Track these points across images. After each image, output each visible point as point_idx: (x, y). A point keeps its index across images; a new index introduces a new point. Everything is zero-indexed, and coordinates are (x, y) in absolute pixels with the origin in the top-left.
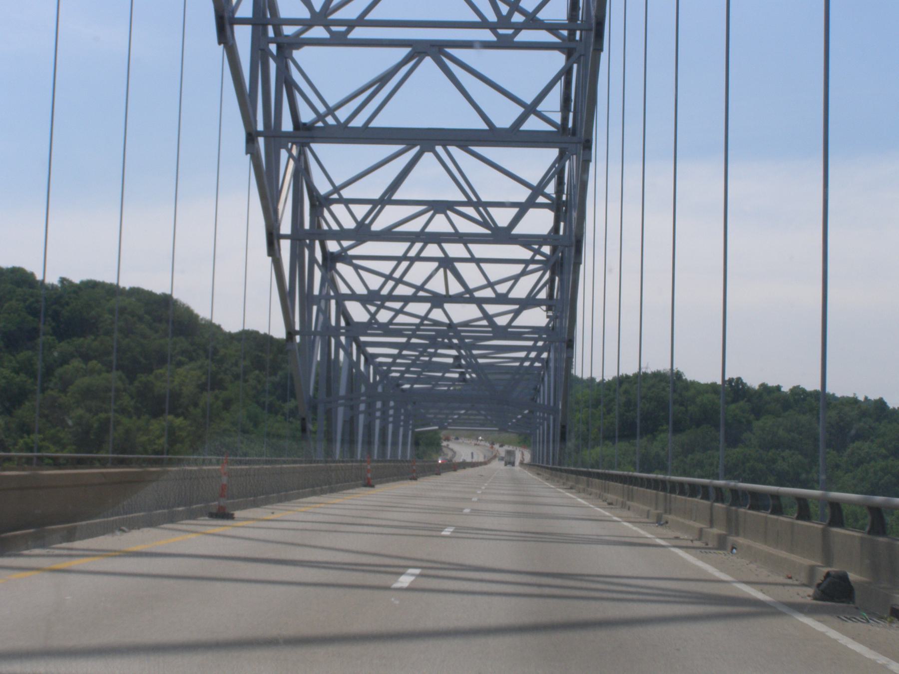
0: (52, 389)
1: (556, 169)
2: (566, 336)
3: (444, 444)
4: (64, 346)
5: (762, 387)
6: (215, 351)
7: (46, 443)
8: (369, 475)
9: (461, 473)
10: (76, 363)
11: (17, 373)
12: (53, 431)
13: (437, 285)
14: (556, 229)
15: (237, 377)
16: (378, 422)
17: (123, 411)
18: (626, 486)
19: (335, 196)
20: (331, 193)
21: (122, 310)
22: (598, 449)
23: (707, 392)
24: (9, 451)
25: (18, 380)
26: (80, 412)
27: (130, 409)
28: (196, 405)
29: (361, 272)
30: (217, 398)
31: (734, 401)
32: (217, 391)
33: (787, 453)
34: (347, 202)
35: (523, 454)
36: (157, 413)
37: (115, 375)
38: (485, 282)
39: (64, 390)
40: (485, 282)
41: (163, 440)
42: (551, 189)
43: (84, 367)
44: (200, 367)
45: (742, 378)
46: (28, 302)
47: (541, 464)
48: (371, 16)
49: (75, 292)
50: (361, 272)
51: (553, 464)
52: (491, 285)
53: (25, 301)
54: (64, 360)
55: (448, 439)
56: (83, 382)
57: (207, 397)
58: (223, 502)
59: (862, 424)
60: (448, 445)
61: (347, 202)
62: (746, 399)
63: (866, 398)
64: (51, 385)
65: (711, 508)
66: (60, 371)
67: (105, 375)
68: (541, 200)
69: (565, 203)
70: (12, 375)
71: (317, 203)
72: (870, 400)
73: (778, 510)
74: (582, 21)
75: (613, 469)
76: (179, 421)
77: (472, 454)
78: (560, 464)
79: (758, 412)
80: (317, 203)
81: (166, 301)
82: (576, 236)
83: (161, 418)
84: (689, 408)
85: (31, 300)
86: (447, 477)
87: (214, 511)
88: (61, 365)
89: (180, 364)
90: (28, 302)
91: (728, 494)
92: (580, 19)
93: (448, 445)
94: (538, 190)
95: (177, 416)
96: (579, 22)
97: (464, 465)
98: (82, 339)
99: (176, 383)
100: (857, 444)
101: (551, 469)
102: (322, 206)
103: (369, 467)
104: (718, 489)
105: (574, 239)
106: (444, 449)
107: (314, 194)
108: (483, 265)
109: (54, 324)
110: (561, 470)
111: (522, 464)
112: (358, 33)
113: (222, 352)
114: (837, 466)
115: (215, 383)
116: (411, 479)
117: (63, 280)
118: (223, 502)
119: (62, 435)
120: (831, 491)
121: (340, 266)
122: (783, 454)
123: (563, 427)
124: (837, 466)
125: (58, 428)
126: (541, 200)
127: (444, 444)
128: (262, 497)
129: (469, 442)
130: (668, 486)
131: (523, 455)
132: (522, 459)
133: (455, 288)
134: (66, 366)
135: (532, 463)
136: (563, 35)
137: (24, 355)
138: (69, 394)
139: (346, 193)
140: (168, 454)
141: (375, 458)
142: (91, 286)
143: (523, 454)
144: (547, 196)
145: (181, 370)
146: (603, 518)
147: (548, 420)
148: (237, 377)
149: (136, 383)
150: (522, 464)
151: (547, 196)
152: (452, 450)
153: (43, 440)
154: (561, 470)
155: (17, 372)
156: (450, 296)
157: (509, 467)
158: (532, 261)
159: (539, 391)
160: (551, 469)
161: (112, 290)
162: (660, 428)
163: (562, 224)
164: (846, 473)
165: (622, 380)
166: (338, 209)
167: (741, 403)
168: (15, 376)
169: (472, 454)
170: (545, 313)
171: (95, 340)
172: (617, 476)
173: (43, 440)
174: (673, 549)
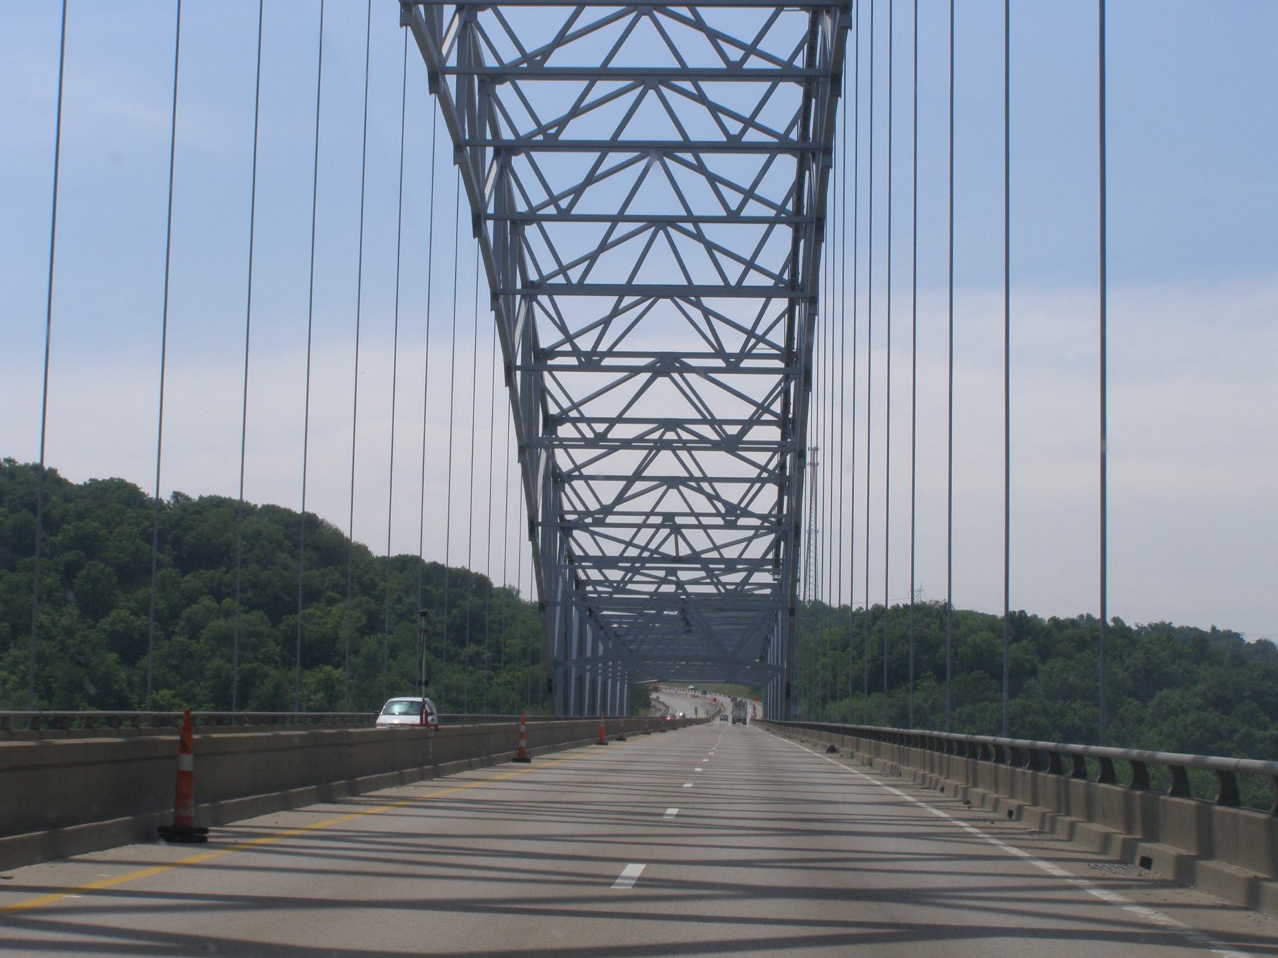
0: (180, 635)
1: (782, 388)
2: (789, 605)
3: (654, 695)
4: (191, 581)
5: (1052, 622)
6: (374, 585)
7: (177, 700)
8: (523, 743)
9: (689, 728)
10: (207, 601)
11: (137, 615)
12: (185, 686)
13: (669, 549)
14: (779, 503)
15: (401, 617)
16: (588, 675)
17: (268, 660)
18: (902, 747)
19: (577, 473)
20: (573, 470)
21: (258, 534)
22: (846, 702)
23: (981, 630)
24: (135, 710)
25: (139, 622)
26: (217, 662)
27: (277, 658)
28: (356, 651)
29: (596, 537)
30: (380, 642)
31: (1017, 639)
32: (379, 635)
33: (1078, 705)
34: (587, 479)
35: (754, 708)
36: (308, 664)
37: (256, 616)
38: (711, 546)
39: (194, 635)
40: (711, 546)
41: (320, 695)
42: (777, 407)
43: (217, 606)
44: (357, 606)
45: (1026, 611)
46: (142, 526)
47: (771, 720)
48: (617, 349)
49: (198, 512)
50: (596, 537)
51: (781, 719)
52: (716, 548)
53: (138, 525)
54: (191, 599)
55: (656, 690)
56: (220, 624)
57: (370, 642)
58: (622, 734)
59: (1175, 667)
60: (658, 698)
61: (587, 479)
62: (1030, 638)
63: (1214, 628)
64: (177, 629)
65: (924, 752)
66: (187, 612)
67: (244, 616)
68: (767, 417)
69: (789, 479)
70: (132, 617)
71: (559, 480)
72: (1218, 631)
73: (1000, 758)
74: (797, 349)
75: (862, 723)
76: (337, 673)
77: (696, 709)
78: (786, 719)
79: (1045, 653)
80: (559, 480)
81: (310, 522)
82: (795, 523)
83: (316, 669)
84: (959, 649)
85: (147, 523)
86: (657, 738)
87: (516, 757)
88: (189, 604)
89: (331, 602)
90: (142, 526)
91: (1008, 752)
92: (795, 348)
93: (658, 698)
94: (763, 408)
95: (337, 666)
96: (794, 351)
97: (685, 722)
98: (212, 571)
99: (329, 626)
100: (1165, 692)
101: (778, 724)
102: (563, 482)
103: (523, 729)
104: (999, 747)
105: (793, 526)
106: (653, 703)
107: (558, 471)
108: (710, 531)
109: (174, 553)
110: (786, 724)
111: (754, 720)
112: (607, 362)
113: (381, 585)
114: (1141, 721)
115: (372, 625)
116: (618, 739)
117: (177, 495)
118: (622, 734)
119: (196, 690)
120: (1158, 750)
121: (576, 533)
122: (1073, 706)
123: (788, 685)
124: (1141, 721)
125: (191, 682)
126: (767, 417)
127: (654, 695)
128: (475, 759)
129: (672, 691)
130: (955, 746)
131: (754, 709)
132: (754, 715)
133: (684, 551)
134: (195, 606)
135: (833, 14)
136: (772, 521)
137: (140, 594)
138: (202, 641)
139: (586, 471)
140: (242, 707)
141: (625, 715)
142: (215, 503)
143: (754, 708)
144: (773, 414)
145: (336, 609)
146: (840, 771)
147: (777, 677)
148: (401, 617)
149: (283, 627)
150: (754, 720)
151: (773, 414)
152: (663, 704)
153: (175, 696)
154: (786, 724)
155: (136, 614)
156: (680, 557)
157: (723, 722)
158: (761, 527)
159: (770, 641)
160: (778, 724)
161: (240, 509)
162: (923, 675)
163: (786, 498)
164: (1151, 728)
165: (878, 613)
166: (580, 485)
167: (1024, 642)
168: (136, 618)
169: (696, 709)
170: (772, 576)
171: (227, 573)
172: (867, 731)
173: (175, 696)
174: (886, 788)
